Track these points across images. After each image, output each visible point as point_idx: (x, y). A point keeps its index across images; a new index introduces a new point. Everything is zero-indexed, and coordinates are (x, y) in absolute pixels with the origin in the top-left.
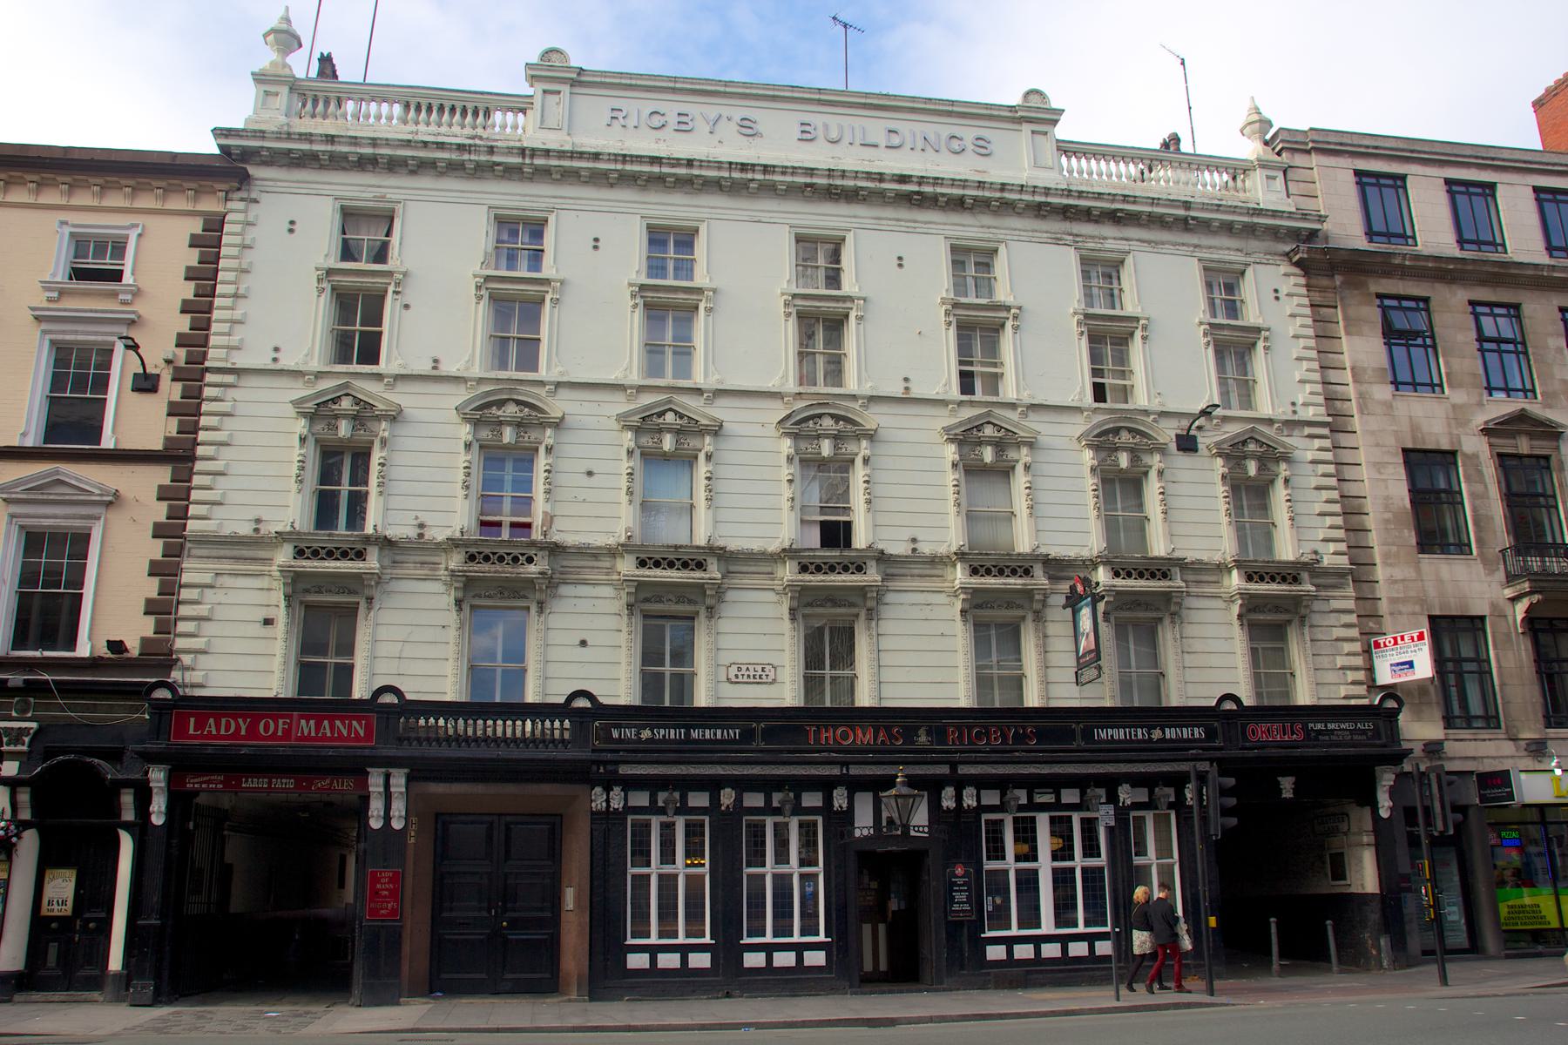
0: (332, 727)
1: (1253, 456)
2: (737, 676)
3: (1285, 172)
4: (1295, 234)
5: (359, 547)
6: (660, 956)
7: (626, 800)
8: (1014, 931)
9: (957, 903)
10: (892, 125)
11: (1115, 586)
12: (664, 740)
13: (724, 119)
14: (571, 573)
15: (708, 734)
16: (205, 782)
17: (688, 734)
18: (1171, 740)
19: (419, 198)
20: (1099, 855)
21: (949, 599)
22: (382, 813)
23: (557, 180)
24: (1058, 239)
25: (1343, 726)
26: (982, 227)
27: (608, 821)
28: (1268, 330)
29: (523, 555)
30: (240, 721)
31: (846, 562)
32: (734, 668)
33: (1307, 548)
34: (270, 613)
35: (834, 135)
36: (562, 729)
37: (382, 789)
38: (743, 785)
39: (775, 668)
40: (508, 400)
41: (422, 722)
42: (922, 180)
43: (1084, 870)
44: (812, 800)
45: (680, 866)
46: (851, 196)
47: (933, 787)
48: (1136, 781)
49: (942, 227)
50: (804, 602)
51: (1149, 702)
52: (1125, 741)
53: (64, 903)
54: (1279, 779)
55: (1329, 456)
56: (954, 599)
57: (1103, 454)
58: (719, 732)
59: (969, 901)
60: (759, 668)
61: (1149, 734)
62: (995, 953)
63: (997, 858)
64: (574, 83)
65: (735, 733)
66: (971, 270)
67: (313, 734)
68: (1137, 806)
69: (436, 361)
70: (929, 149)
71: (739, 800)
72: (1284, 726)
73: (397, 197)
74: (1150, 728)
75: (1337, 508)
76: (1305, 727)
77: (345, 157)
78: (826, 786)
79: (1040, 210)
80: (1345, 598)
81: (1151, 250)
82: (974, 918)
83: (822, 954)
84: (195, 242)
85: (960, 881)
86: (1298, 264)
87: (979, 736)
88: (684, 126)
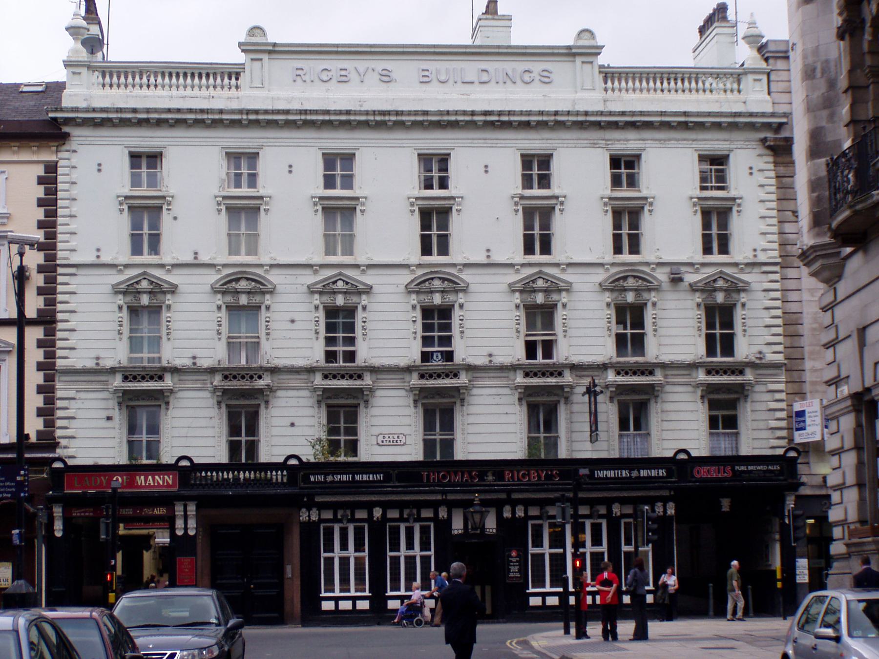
0: (154, 479)
1: (721, 289)
2: (383, 442)
3: (769, 75)
4: (767, 126)
5: (160, 373)
6: (340, 602)
7: (319, 515)
8: (548, 589)
9: (513, 572)
10: (484, 65)
11: (616, 381)
12: (340, 482)
13: (370, 70)
14: (283, 383)
15: (365, 478)
16: (83, 512)
17: (353, 478)
18: (644, 477)
19: (102, 143)
20: (601, 545)
21: (512, 391)
22: (183, 526)
23: (264, 126)
24: (595, 144)
25: (759, 468)
26: (543, 139)
27: (310, 531)
28: (741, 198)
29: (255, 374)
30: (102, 478)
31: (447, 372)
32: (381, 436)
33: (755, 349)
34: (110, 413)
35: (443, 78)
36: (283, 476)
37: (183, 513)
38: (386, 506)
39: (405, 436)
40: (242, 278)
41: (203, 474)
42: (500, 113)
43: (592, 554)
44: (427, 513)
45: (351, 553)
46: (454, 125)
47: (498, 505)
48: (623, 501)
49: (514, 141)
50: (422, 396)
51: (734, 453)
52: (615, 478)
53: (7, 580)
54: (721, 499)
55: (777, 286)
56: (515, 391)
57: (616, 294)
58: (371, 476)
59: (519, 571)
60: (396, 436)
61: (630, 473)
62: (535, 601)
63: (537, 546)
64: (270, 52)
65: (380, 477)
66: (535, 171)
67: (143, 484)
68: (624, 516)
69: (196, 253)
70: (509, 82)
71: (384, 514)
72: (719, 468)
73: (164, 143)
74: (326, 475)
75: (779, 322)
76: (733, 470)
77: (129, 120)
78: (434, 505)
79: (581, 126)
80: (779, 382)
81: (659, 146)
82: (522, 581)
83: (557, 598)
84: (41, 181)
85: (514, 560)
86: (769, 148)
87: (524, 476)
88: (344, 80)
